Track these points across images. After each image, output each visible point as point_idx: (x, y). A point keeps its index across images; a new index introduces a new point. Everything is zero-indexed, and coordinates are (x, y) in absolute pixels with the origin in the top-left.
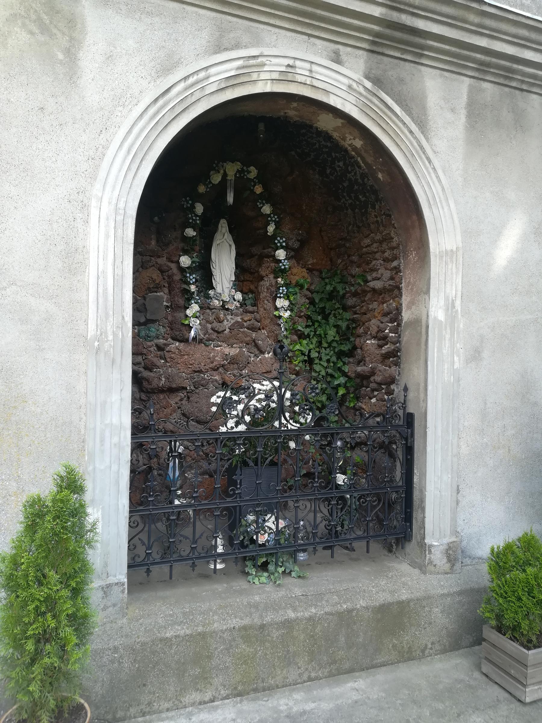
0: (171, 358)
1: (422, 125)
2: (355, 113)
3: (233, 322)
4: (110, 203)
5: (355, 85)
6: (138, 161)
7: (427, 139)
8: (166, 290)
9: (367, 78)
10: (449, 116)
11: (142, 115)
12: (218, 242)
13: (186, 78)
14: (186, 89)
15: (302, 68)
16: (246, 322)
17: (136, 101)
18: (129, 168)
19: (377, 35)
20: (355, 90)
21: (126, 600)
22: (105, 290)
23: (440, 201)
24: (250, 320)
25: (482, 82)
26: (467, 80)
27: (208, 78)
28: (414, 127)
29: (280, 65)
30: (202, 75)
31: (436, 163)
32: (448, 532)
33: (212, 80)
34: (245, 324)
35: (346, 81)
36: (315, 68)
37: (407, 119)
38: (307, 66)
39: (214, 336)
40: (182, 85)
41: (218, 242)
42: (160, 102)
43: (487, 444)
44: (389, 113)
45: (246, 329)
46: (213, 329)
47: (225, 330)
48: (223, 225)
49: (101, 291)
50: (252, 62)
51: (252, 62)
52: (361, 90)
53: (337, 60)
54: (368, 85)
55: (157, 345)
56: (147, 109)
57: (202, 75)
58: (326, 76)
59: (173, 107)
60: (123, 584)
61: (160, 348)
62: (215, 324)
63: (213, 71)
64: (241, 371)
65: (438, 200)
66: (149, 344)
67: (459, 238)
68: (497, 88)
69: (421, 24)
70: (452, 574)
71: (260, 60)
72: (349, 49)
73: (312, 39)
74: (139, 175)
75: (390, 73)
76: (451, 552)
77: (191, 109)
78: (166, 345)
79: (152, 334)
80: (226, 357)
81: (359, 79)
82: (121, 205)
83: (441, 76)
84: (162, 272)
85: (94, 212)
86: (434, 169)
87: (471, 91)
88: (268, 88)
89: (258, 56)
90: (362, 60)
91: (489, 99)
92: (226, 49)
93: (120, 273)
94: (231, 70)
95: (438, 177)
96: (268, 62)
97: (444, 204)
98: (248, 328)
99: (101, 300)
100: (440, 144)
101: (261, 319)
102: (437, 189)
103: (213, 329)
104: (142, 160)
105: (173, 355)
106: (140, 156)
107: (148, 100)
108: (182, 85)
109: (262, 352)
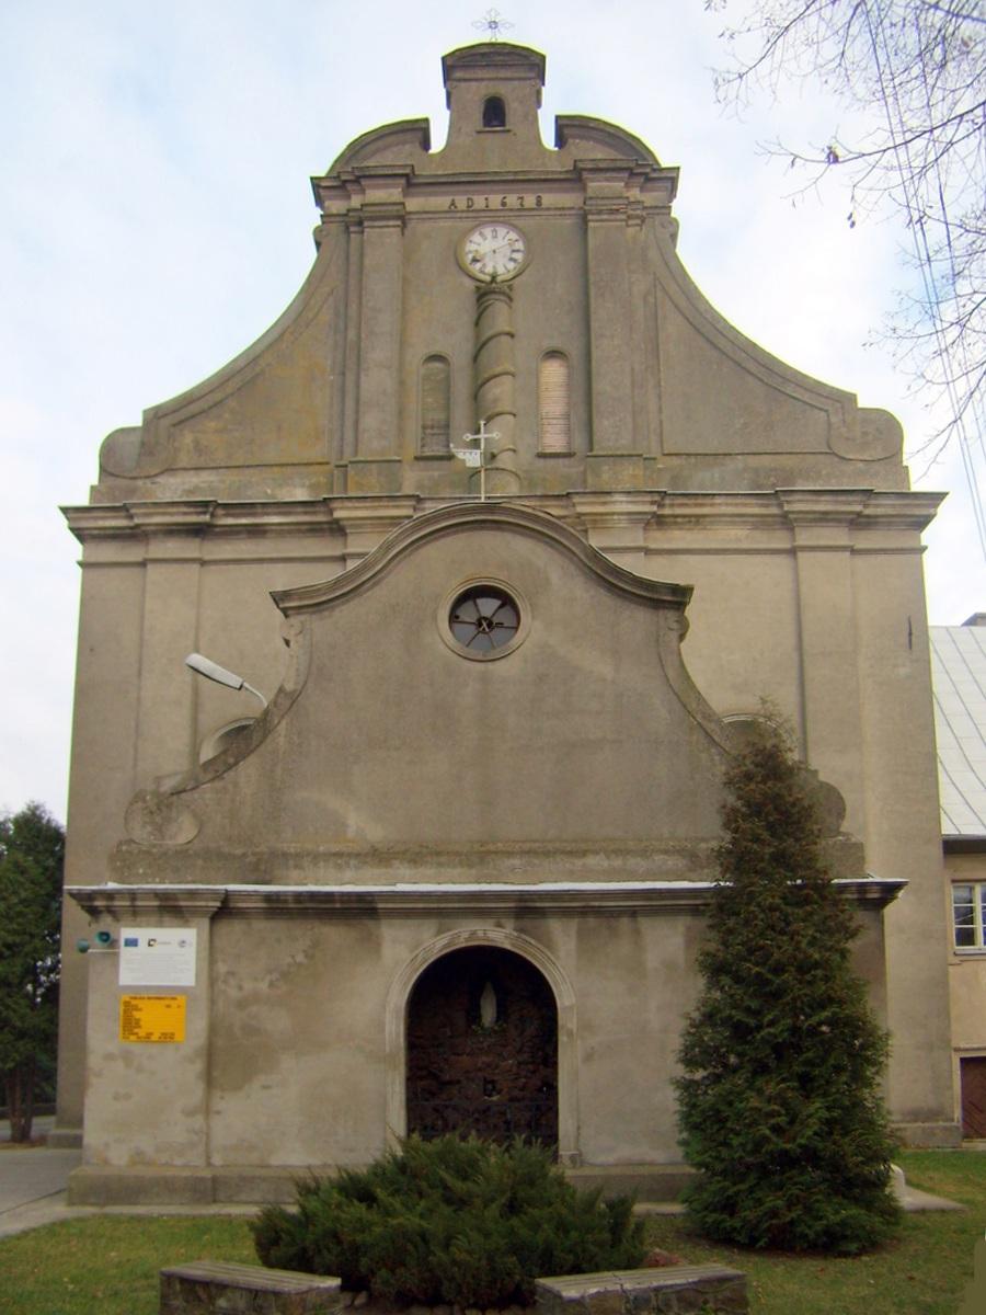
1: (549, 947)
7: (552, 953)
15: (480, 934)
29: (466, 935)
37: (539, 946)
48: (489, 986)
53: (499, 925)
54: (516, 934)
69: (538, 905)
88: (464, 945)
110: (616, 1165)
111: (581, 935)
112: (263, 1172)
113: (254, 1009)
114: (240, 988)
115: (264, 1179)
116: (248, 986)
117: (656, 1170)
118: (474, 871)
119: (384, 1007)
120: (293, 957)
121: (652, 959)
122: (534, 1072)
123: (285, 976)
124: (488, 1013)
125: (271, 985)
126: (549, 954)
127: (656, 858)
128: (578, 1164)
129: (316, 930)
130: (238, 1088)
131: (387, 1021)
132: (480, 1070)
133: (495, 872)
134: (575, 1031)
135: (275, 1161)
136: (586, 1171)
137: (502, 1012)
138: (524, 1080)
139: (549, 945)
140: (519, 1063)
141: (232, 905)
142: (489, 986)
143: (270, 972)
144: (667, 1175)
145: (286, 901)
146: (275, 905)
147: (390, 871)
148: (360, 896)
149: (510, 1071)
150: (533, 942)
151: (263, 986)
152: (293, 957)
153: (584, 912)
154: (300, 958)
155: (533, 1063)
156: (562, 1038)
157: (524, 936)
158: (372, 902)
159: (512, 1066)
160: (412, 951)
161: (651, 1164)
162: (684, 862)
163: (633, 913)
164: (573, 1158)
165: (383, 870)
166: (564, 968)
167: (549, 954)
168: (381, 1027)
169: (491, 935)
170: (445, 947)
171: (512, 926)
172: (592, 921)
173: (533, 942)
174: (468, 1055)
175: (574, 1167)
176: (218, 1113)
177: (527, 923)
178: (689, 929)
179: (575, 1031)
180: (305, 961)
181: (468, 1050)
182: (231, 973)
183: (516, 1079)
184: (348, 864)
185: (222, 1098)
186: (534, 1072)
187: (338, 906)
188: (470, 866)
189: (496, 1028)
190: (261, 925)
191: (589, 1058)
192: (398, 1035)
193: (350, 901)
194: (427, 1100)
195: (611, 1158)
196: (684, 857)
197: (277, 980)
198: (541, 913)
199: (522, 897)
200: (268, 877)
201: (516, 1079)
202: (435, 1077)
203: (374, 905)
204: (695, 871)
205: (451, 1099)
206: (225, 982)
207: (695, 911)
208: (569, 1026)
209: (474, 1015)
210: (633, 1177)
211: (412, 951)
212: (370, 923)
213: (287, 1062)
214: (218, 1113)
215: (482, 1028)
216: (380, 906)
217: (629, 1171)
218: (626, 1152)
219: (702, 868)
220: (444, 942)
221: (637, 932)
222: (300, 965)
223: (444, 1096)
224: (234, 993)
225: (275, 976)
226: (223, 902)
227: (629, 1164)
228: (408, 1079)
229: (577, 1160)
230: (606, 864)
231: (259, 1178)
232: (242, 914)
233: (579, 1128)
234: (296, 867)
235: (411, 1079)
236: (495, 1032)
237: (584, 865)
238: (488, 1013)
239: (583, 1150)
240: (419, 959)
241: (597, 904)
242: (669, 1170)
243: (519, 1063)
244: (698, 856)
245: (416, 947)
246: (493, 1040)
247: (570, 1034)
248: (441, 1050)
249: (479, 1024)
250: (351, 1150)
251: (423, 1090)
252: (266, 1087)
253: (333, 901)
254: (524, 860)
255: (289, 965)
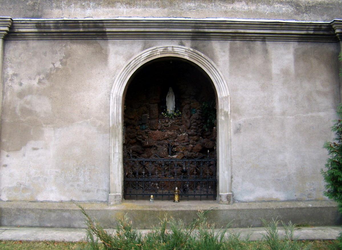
0: (150, 136)
1: (212, 58)
2: (188, 58)
3: (172, 122)
4: (115, 94)
5: (187, 51)
6: (123, 82)
7: (215, 62)
8: (148, 113)
9: (192, 47)
10: (223, 54)
11: (123, 70)
12: (168, 95)
13: (135, 59)
14: (135, 61)
15: (170, 49)
16: (176, 122)
17: (122, 67)
18: (120, 85)
19: (192, 35)
20: (187, 52)
21: (121, 200)
22: (114, 117)
23: (221, 81)
24: (178, 122)
25: (235, 41)
26: (229, 41)
27: (141, 57)
28: (209, 60)
29: (161, 50)
30: (140, 57)
31: (218, 70)
32: (228, 191)
33: (142, 58)
34: (176, 123)
35: (184, 50)
36: (174, 48)
37: (206, 58)
38: (171, 48)
39: (165, 128)
40: (134, 61)
41: (168, 95)
42: (128, 66)
43: (243, 162)
44: (200, 57)
45: (177, 125)
46: (164, 125)
47: (169, 126)
48: (171, 89)
49: (113, 117)
50: (154, 51)
51: (154, 51)
52: (190, 52)
53: (182, 44)
54: (192, 50)
55: (145, 132)
56: (125, 68)
57: (140, 57)
58: (177, 50)
59: (132, 67)
60: (120, 195)
61: (146, 133)
62: (165, 124)
63: (143, 55)
64: (174, 140)
65: (219, 81)
66: (143, 131)
67: (228, 92)
68: (241, 42)
69: (206, 30)
70: (229, 204)
71: (156, 49)
72: (185, 41)
73: (173, 40)
74: (123, 86)
75: (200, 45)
76: (228, 197)
77: (137, 66)
78: (148, 131)
79: (144, 128)
80: (168, 135)
81: (188, 49)
82: (118, 94)
83: (219, 42)
84: (147, 107)
85: (111, 97)
86: (217, 71)
87: (231, 44)
88: (159, 56)
89: (156, 49)
90: (190, 43)
91: (238, 46)
92: (147, 49)
93: (118, 112)
94: (148, 54)
95: (219, 74)
96: (159, 50)
97: (222, 82)
98: (178, 125)
99: (113, 120)
100: (220, 63)
101: (182, 121)
102: (218, 78)
103: (164, 125)
104: (124, 82)
105: (151, 135)
106: (123, 81)
107: (125, 66)
108: (134, 61)
109: (181, 133)
110: (255, 202)
111: (232, 51)
112: (33, 206)
113: (29, 98)
114: (21, 84)
115: (32, 210)
116: (25, 83)
117: (280, 205)
118: (166, 10)
119: (109, 96)
120: (53, 64)
121: (275, 68)
122: (197, 141)
123: (48, 76)
124: (171, 106)
125: (40, 82)
126: (213, 63)
127: (276, 6)
128: (231, 202)
129: (68, 47)
130: (18, 149)
131: (111, 105)
132: (166, 139)
133: (179, 11)
134: (229, 113)
135: (40, 198)
136: (237, 206)
137: (178, 105)
138: (192, 146)
139: (213, 58)
140: (189, 135)
141: (16, 30)
142: (171, 89)
143: (39, 74)
144: (287, 209)
145: (49, 28)
146: (43, 30)
147: (115, 9)
148: (96, 23)
149: (184, 140)
150: (203, 55)
151: (35, 83)
152: (53, 64)
153: (234, 37)
154: (58, 65)
155: (196, 135)
156: (221, 118)
157: (197, 51)
158: (103, 27)
159: (185, 136)
160: (127, 60)
161: (276, 201)
162: (292, 9)
163: (264, 38)
164: (228, 198)
165: (111, 9)
166: (221, 72)
167: (213, 63)
168: (107, 109)
169: (176, 50)
170: (148, 57)
171: (190, 44)
172: (238, 43)
173: (203, 55)
174: (159, 130)
175: (229, 203)
176: (6, 166)
177: (200, 43)
178: (296, 50)
179: (229, 113)
180: (61, 66)
181: (159, 127)
182: (15, 75)
183: (187, 145)
184: (88, 5)
185: (8, 156)
186: (197, 141)
187: (81, 30)
188: (164, 7)
189: (175, 114)
190: (34, 44)
191: (238, 131)
192: (118, 114)
193: (89, 27)
194: (136, 157)
195: (251, 197)
196: (292, 6)
197: (43, 79)
198: (206, 36)
199: (197, 24)
200: (40, 14)
201: (187, 145)
202: (139, 143)
203: (104, 30)
204: (299, 15)
205: (149, 157)
206: (11, 80)
207: (302, 39)
208: (226, 110)
209: (163, 107)
210: (266, 210)
211: (127, 60)
212: (102, 43)
213: (48, 133)
214: (6, 166)
215: (167, 114)
216: (108, 30)
217: (264, 206)
218: (261, 193)
219: (303, 13)
220: (148, 54)
221: (266, 51)
222: (57, 69)
223: (145, 155)
224: (16, 87)
225: (42, 76)
226: (10, 28)
227: (262, 201)
228: (124, 145)
229: (230, 199)
230: (246, 8)
231: (30, 209)
232: (23, 36)
233: (232, 177)
234: (57, 7)
235: (126, 145)
236: (175, 116)
237: (232, 8)
238: (171, 106)
239: (235, 192)
240: (132, 65)
241: (242, 31)
242: (288, 205)
243: (189, 135)
244: (300, 6)
245: (130, 58)
246: (174, 121)
247: (226, 115)
248: (144, 127)
249: (166, 112)
250: (88, 191)
251: (133, 151)
252: (35, 149)
253: (78, 27)
254: (54, 239)
255: (51, 69)
